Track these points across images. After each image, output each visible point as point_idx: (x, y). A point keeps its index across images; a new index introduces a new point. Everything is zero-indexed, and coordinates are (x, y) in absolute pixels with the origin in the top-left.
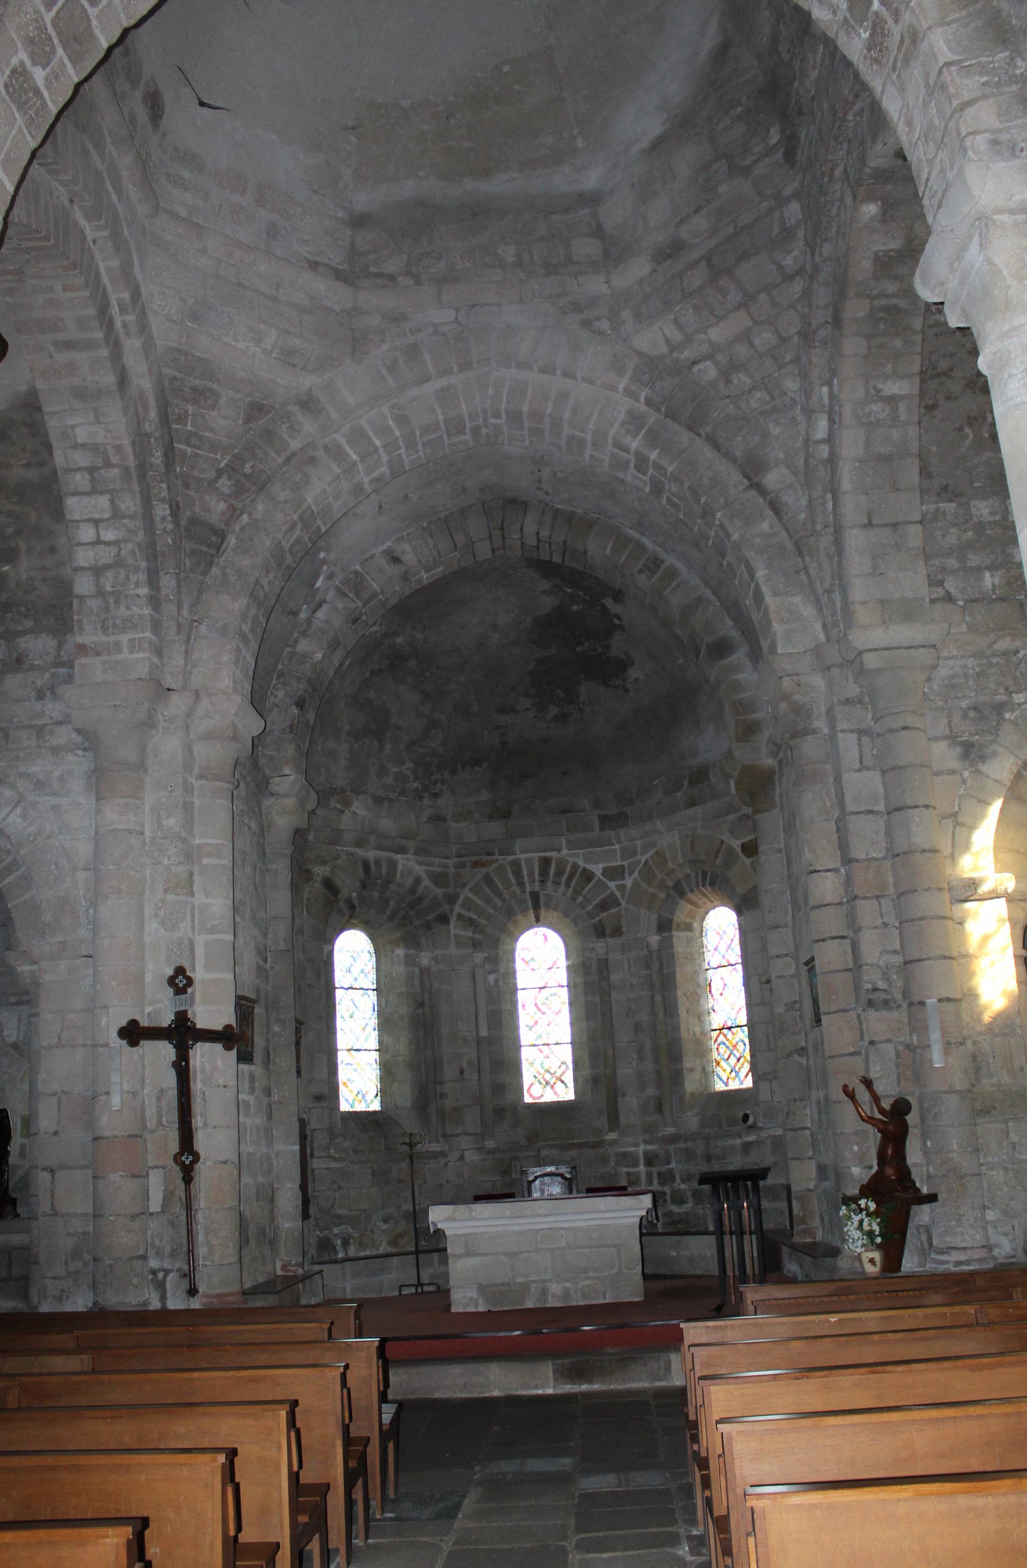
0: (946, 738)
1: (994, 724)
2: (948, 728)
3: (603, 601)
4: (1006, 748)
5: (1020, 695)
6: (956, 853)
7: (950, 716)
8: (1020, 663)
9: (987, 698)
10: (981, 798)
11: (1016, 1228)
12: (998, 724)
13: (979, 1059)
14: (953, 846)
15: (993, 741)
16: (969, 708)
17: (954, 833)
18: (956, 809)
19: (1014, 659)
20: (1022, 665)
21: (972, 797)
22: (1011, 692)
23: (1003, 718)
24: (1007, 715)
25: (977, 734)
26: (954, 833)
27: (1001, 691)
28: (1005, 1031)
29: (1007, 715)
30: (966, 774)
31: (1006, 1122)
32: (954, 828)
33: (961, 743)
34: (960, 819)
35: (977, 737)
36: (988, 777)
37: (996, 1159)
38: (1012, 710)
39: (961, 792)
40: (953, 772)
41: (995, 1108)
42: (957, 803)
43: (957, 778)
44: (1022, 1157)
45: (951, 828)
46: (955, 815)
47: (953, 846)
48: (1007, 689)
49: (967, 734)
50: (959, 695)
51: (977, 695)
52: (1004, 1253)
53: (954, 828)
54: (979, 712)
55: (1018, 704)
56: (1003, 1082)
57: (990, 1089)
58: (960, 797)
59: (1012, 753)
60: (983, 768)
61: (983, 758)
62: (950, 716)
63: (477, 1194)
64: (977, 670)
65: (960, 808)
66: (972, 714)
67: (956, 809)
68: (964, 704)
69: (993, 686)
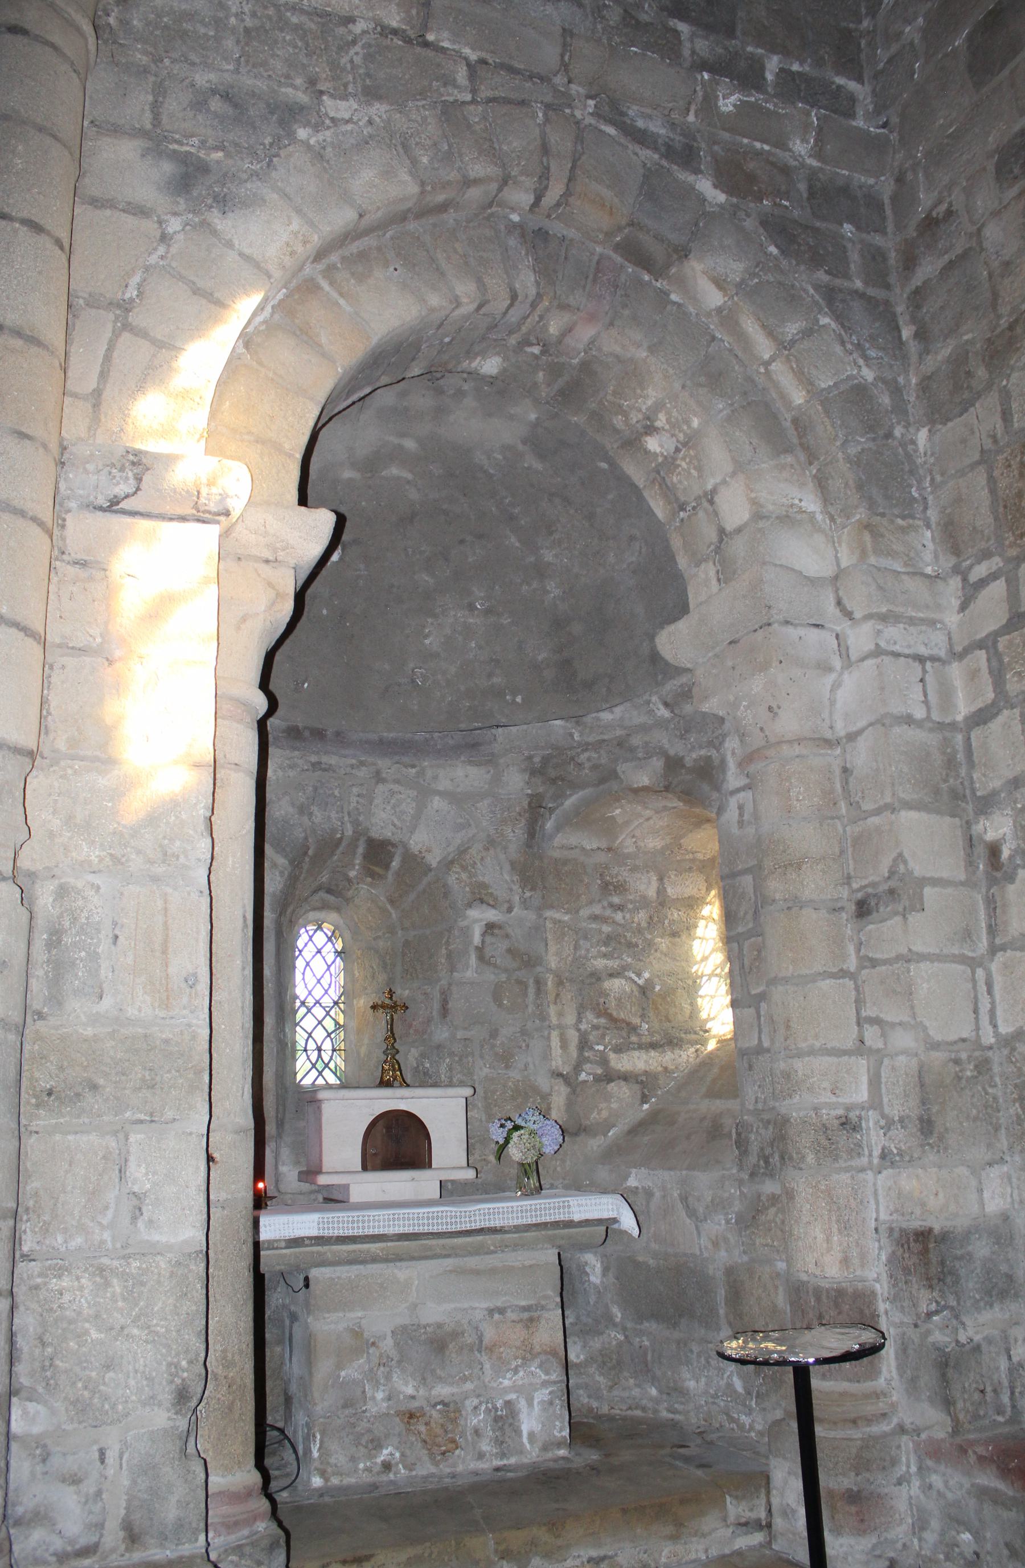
0: (141, 133)
1: (268, 140)
2: (148, 115)
3: (1003, 579)
4: (286, 196)
5: (342, 104)
6: (107, 394)
7: (160, 91)
8: (354, 42)
9: (262, 85)
10: (200, 283)
11: (111, 1456)
12: (277, 141)
13: (67, 940)
14: (103, 375)
15: (255, 175)
16: (214, 92)
17: (110, 350)
18: (132, 293)
19: (341, 30)
20: (357, 48)
21: (181, 278)
22: (322, 93)
23: (291, 135)
24: (302, 133)
25: (222, 148)
26: (110, 350)
27: (299, 81)
28: (160, 870)
29: (302, 133)
30: (174, 225)
31: (121, 1132)
32: (116, 335)
33: (174, 156)
34: (131, 318)
35: (220, 154)
36: (229, 245)
37: (78, 1240)
38: (317, 128)
39: (153, 259)
40: (141, 211)
41: (94, 1087)
42: (136, 279)
43: (149, 226)
44: (156, 1237)
45: (108, 334)
46: (125, 307)
47: (103, 375)
48: (312, 82)
49: (195, 141)
50: (193, 57)
51: (237, 71)
52: (58, 1544)
53: (116, 335)
54: (236, 106)
55: (333, 120)
56: (131, 1012)
57: (89, 1032)
58: (147, 269)
59: (299, 211)
60: (215, 217)
61: (223, 203)
62: (160, 91)
63: (294, 495)
64: (249, 22)
65: (140, 294)
66: (216, 104)
67: (132, 293)
68: (203, 78)
69: (278, 65)
